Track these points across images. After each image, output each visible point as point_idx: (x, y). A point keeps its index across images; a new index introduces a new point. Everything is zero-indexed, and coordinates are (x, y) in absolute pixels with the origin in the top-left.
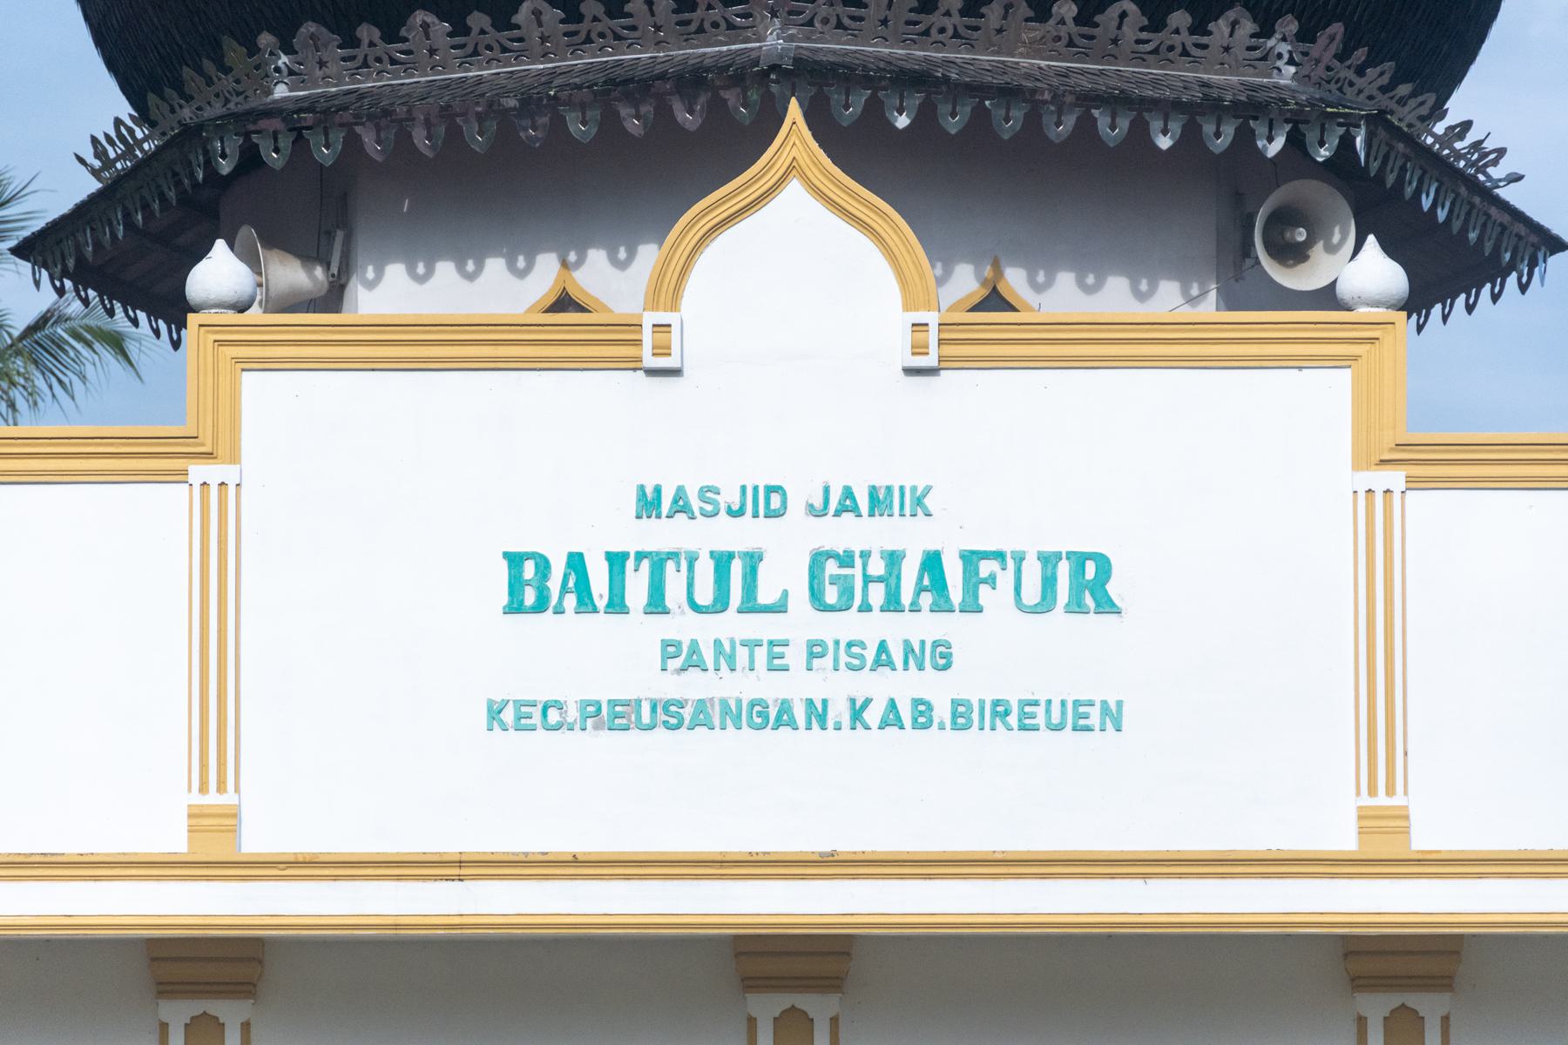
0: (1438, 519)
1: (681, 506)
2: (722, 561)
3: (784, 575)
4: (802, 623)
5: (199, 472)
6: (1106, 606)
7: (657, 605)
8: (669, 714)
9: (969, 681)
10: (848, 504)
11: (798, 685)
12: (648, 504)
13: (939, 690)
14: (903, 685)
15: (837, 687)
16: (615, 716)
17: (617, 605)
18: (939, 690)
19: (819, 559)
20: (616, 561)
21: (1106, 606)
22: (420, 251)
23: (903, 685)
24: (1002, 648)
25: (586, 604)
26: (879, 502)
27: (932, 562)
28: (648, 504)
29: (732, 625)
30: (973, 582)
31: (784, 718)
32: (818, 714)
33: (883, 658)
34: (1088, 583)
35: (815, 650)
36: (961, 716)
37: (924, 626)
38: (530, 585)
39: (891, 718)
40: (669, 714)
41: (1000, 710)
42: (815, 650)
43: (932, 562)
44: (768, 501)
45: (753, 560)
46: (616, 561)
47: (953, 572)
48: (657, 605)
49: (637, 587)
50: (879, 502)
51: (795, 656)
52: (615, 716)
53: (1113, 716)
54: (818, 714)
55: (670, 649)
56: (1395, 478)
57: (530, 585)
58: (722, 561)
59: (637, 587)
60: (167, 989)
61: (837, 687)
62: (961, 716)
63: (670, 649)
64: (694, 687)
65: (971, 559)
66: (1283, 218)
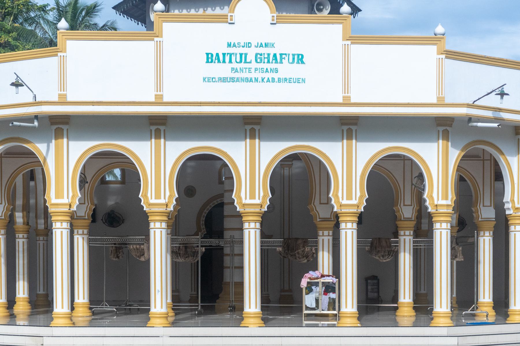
0: (356, 49)
1: (234, 46)
2: (241, 55)
3: (251, 57)
4: (254, 65)
5: (156, 39)
6: (303, 63)
7: (230, 62)
8: (232, 80)
9: (281, 75)
10: (261, 46)
11: (253, 75)
12: (229, 45)
13: (276, 76)
14: (270, 75)
15: (259, 75)
16: (224, 80)
17: (224, 62)
18: (276, 76)
19: (257, 54)
20: (224, 54)
21: (303, 63)
22: (181, 8)
23: (270, 75)
24: (286, 69)
25: (219, 62)
26: (266, 45)
27: (275, 55)
28: (229, 45)
29: (243, 65)
30: (281, 58)
31: (251, 81)
32: (256, 80)
33: (267, 71)
34: (300, 59)
35: (256, 69)
36: (279, 80)
37: (273, 66)
38: (210, 58)
39: (268, 81)
40: (232, 80)
41: (286, 79)
42: (256, 69)
43: (275, 55)
44: (248, 45)
45: (246, 55)
46: (224, 54)
47: (278, 57)
48: (230, 62)
49: (227, 59)
50: (266, 45)
51: (253, 70)
52: (224, 80)
53: (304, 81)
54: (256, 80)
55: (233, 69)
56: (349, 42)
57: (210, 58)
58: (241, 55)
59: (227, 59)
60: (152, 124)
61: (259, 75)
62: (279, 80)
63: (233, 69)
64: (236, 75)
65: (281, 55)
66: (319, 4)
